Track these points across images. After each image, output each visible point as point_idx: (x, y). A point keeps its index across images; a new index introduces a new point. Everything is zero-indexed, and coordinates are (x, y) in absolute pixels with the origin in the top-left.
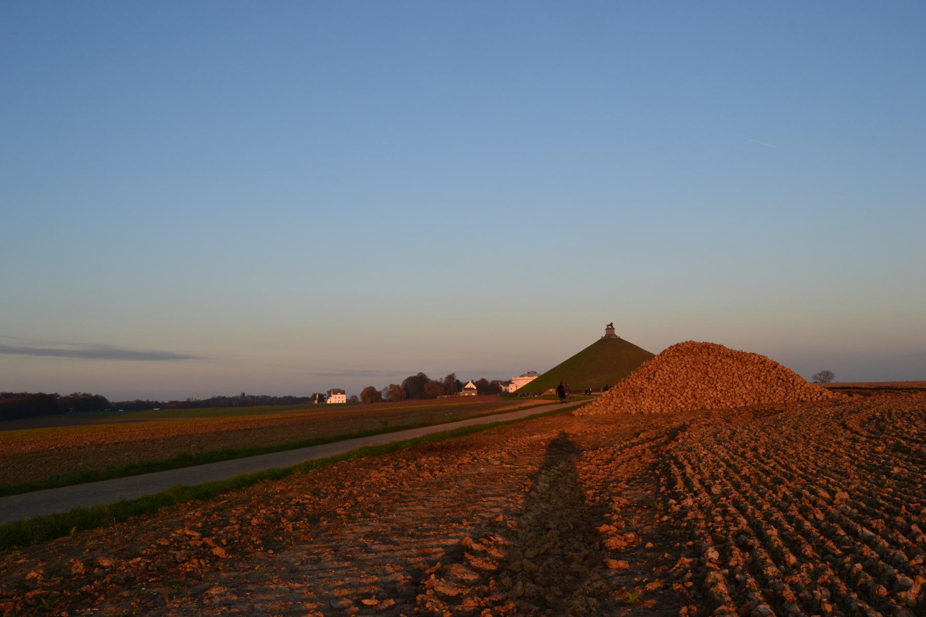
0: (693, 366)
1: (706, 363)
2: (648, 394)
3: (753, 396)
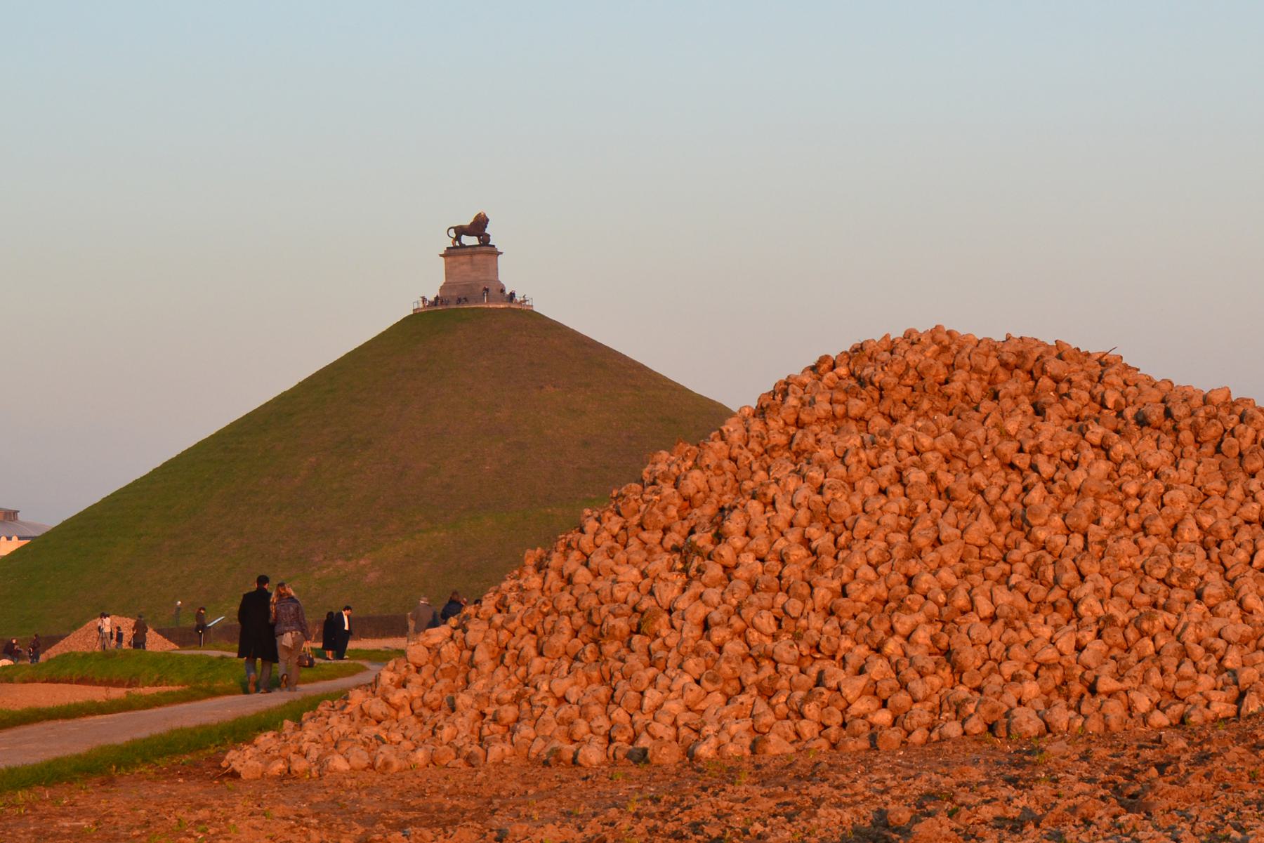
0: (946, 479)
1: (1022, 461)
2: (682, 641)
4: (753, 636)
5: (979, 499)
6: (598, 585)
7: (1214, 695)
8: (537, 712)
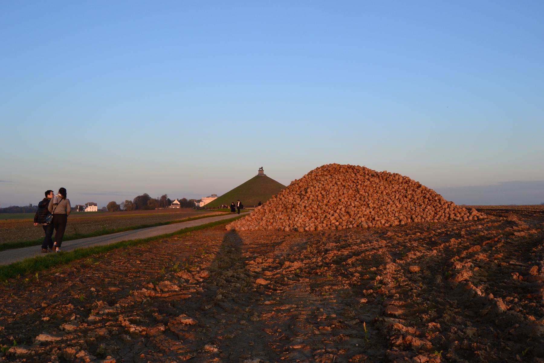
0: (344, 184)
1: (355, 181)
2: (301, 209)
3: (405, 213)
4: (313, 209)
5: (349, 187)
6: (286, 200)
8: (276, 221)
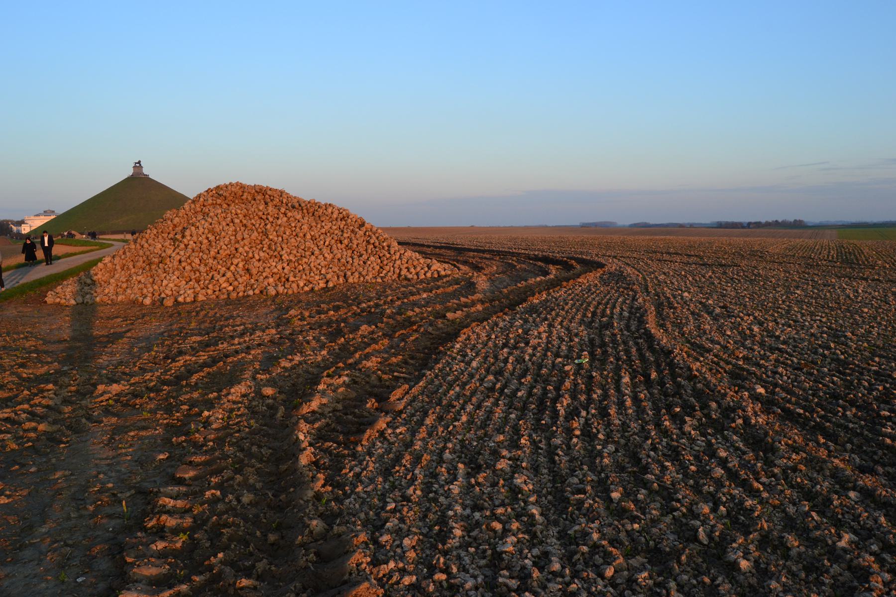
0: (245, 222)
1: (264, 217)
4: (193, 264)
7: (320, 281)
